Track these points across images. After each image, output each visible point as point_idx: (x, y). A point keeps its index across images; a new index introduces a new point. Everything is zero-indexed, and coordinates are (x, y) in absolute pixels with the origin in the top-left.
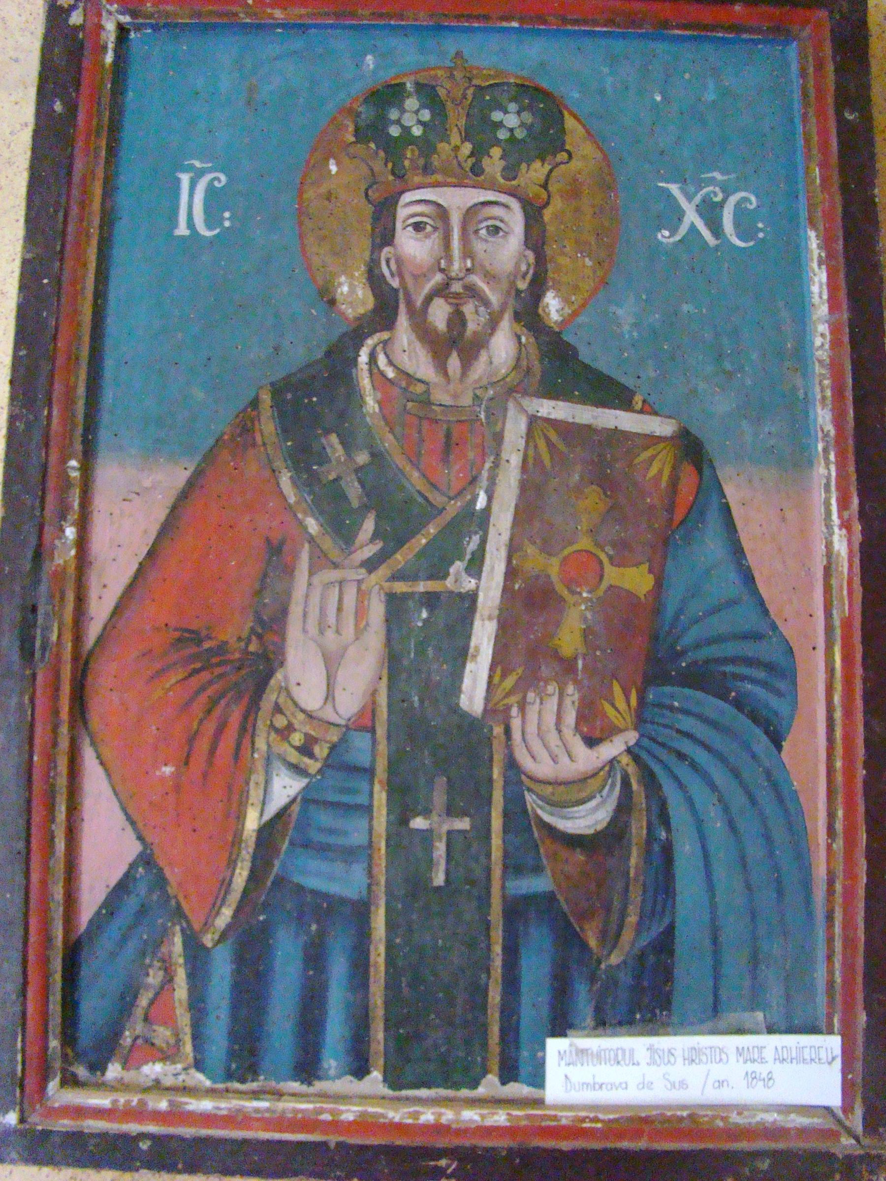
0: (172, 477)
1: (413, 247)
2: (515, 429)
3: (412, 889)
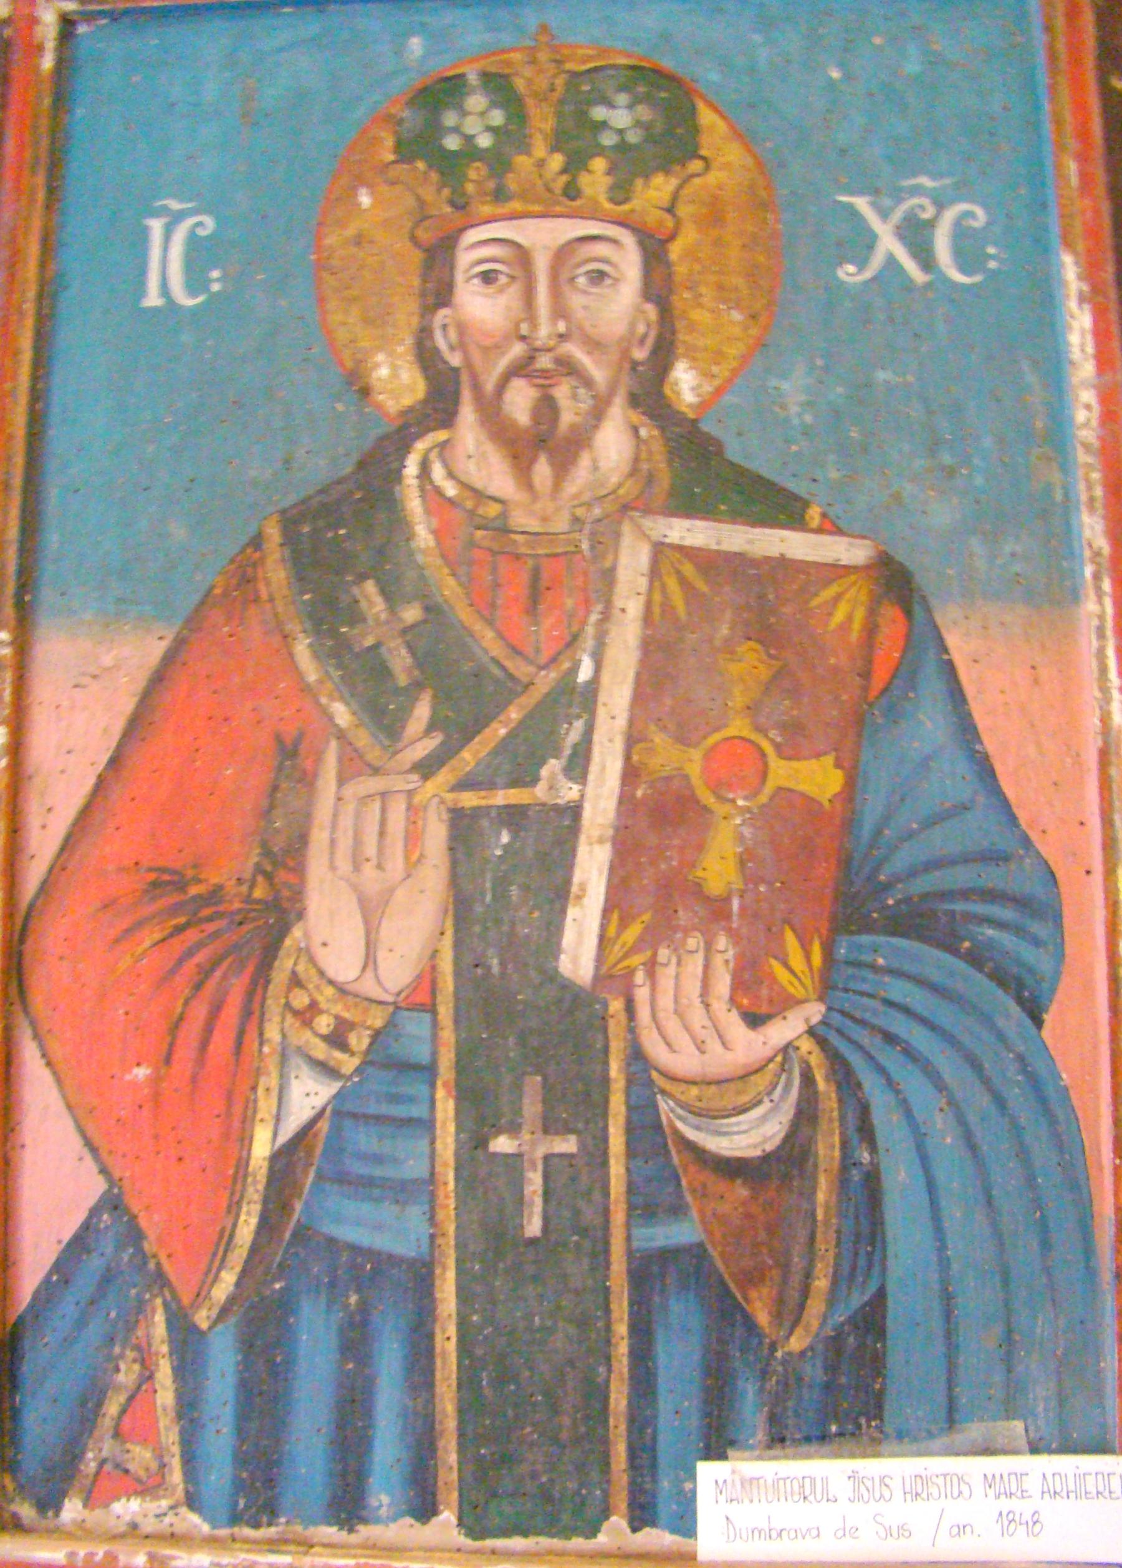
0: (140, 651)
1: (480, 307)
2: (632, 562)
3: (491, 1239)
